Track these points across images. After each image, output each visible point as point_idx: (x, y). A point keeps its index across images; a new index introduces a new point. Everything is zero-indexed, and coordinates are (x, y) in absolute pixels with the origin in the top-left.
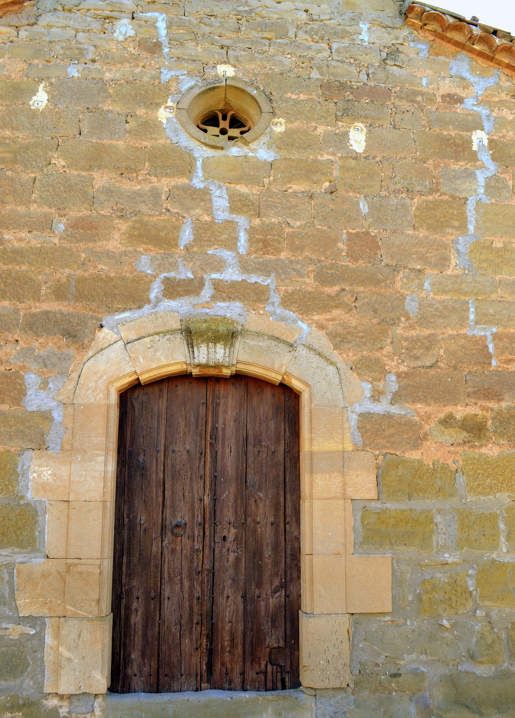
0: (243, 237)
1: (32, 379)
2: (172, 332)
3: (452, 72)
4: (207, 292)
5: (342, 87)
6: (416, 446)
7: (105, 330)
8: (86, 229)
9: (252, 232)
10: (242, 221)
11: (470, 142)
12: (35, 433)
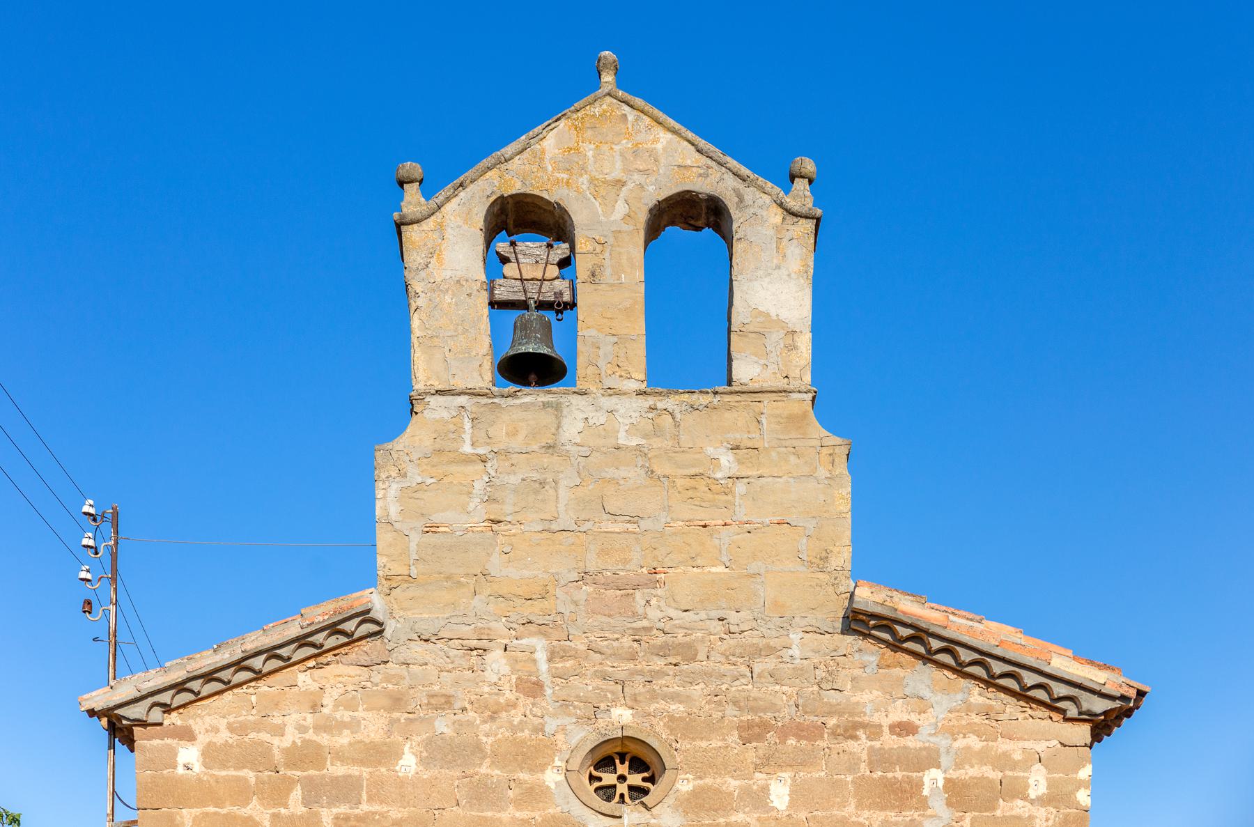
3: (908, 691)
5: (765, 727)
11: (920, 785)
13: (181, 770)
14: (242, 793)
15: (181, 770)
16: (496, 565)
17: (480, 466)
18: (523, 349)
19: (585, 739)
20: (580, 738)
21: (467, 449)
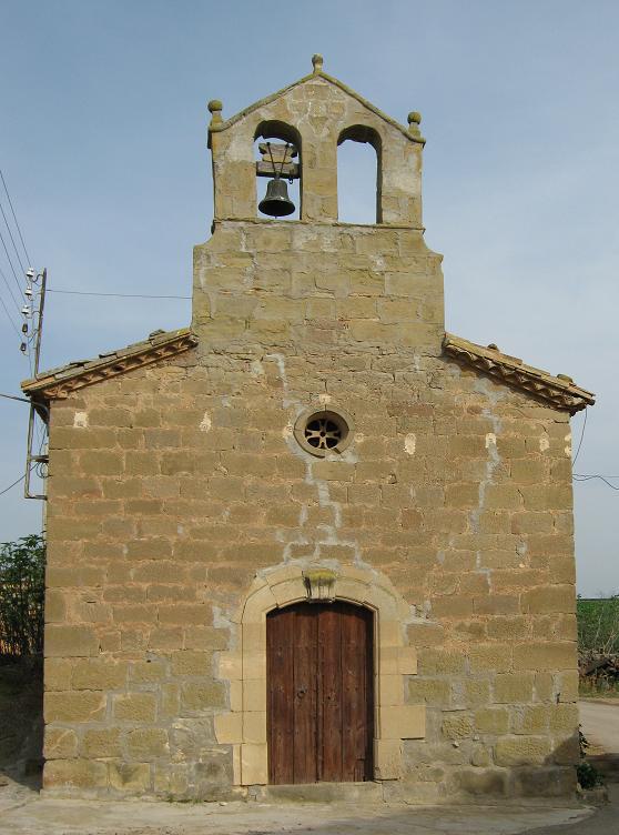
0: (338, 516)
1: (216, 610)
2: (297, 579)
4: (317, 553)
6: (441, 643)
7: (257, 578)
8: (243, 514)
9: (344, 512)
10: (337, 505)
12: (221, 641)
13: (75, 426)
14: (109, 439)
15: (75, 426)
16: (257, 313)
17: (250, 260)
18: (276, 198)
19: (303, 414)
20: (303, 412)
21: (243, 250)
